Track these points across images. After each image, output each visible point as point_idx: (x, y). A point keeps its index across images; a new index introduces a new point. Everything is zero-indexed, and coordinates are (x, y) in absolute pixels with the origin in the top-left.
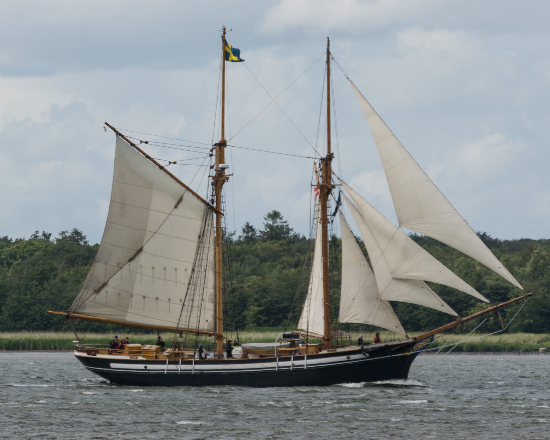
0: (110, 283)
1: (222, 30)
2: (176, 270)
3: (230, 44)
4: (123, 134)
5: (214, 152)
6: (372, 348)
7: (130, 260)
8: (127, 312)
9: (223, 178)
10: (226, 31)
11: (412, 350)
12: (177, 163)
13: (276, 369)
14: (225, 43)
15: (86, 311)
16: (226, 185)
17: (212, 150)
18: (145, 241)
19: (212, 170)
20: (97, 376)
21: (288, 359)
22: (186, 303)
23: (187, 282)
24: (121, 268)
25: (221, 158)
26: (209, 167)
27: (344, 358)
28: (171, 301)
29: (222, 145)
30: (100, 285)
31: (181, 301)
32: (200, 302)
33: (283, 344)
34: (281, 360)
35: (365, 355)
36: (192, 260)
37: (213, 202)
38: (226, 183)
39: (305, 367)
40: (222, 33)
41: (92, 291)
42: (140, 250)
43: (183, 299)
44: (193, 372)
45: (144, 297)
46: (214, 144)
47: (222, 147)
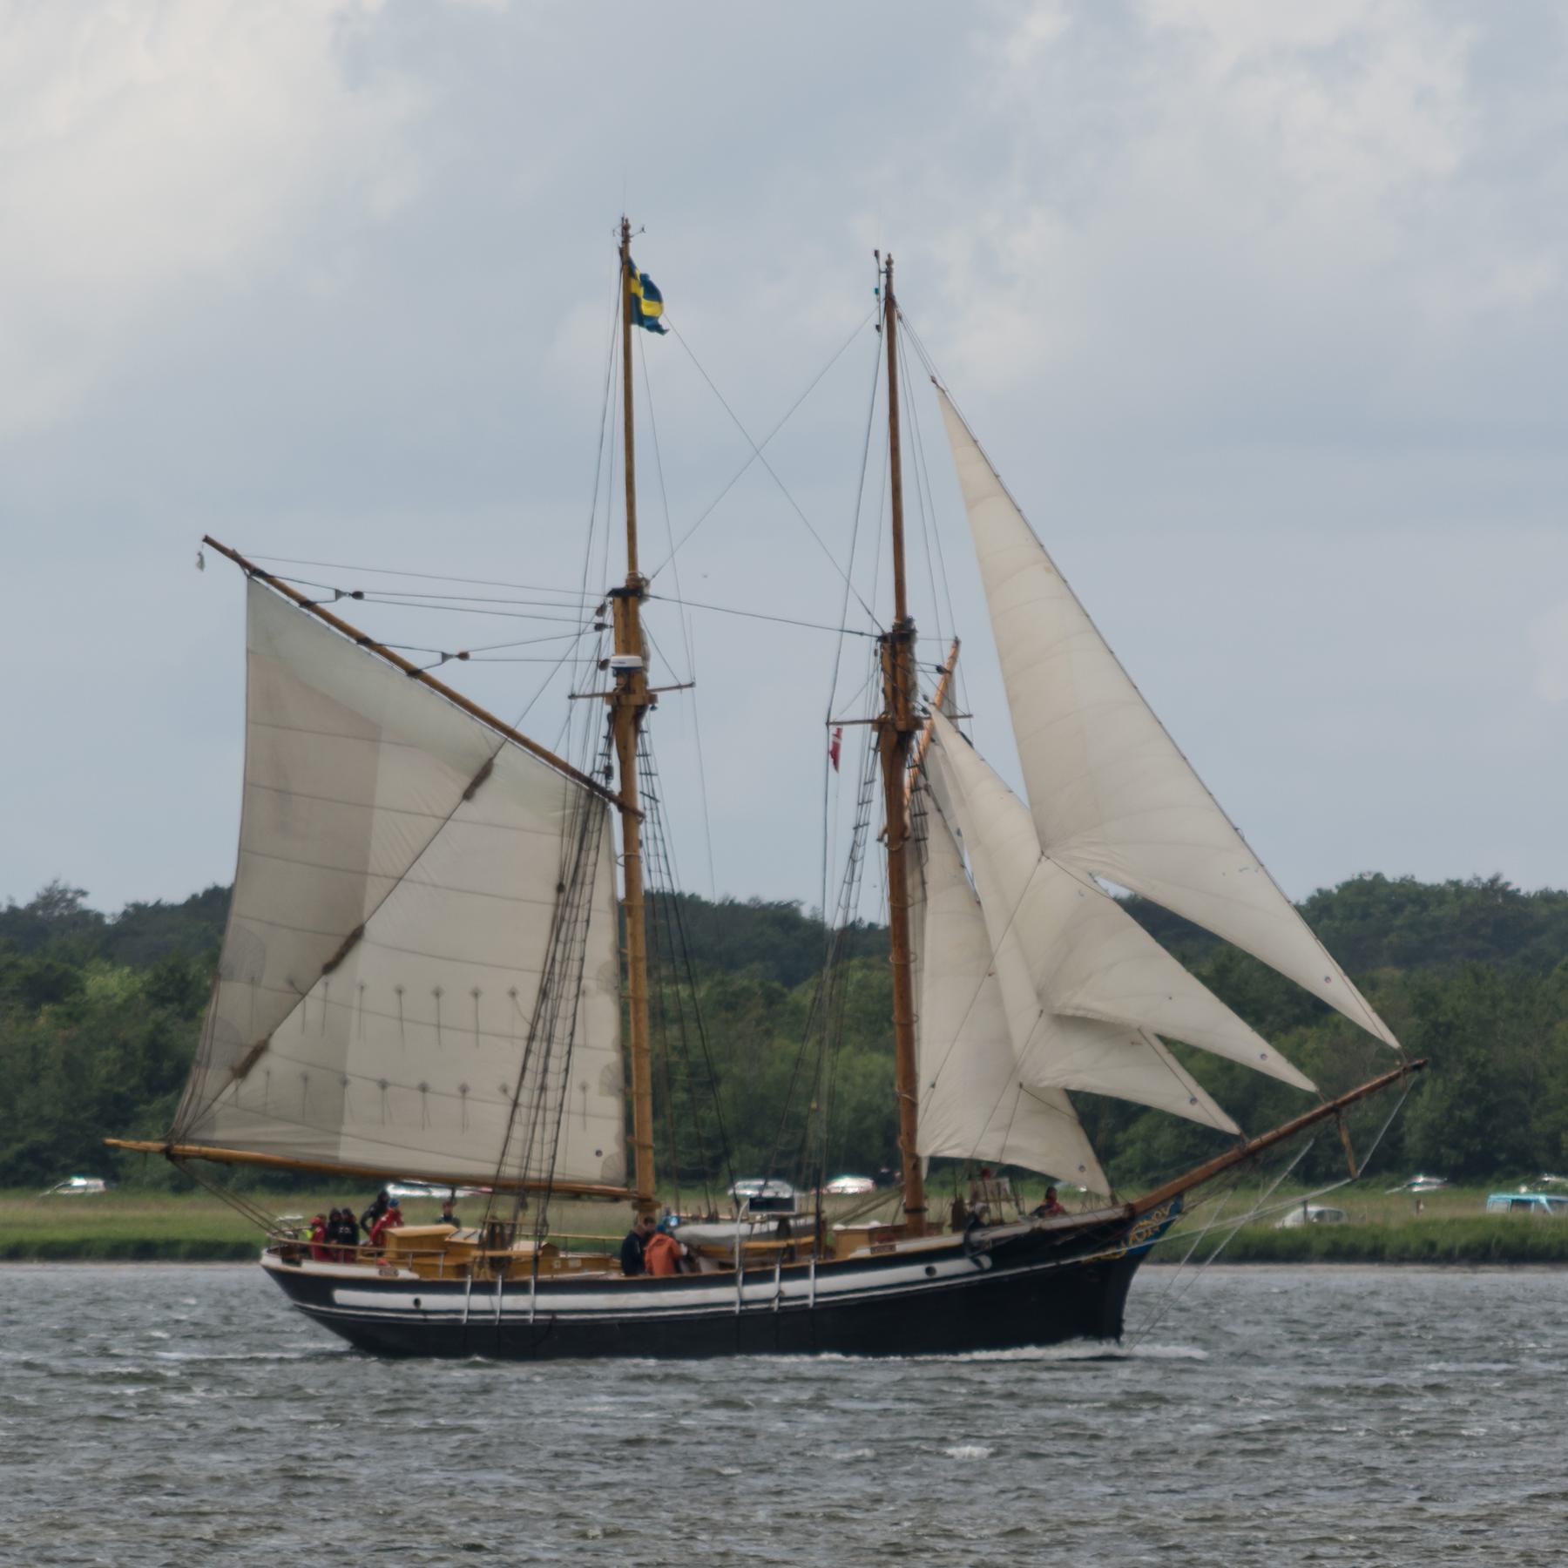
0: (276, 1043)
1: (619, 230)
2: (476, 994)
3: (640, 269)
4: (268, 571)
5: (609, 618)
6: (994, 1241)
7: (330, 967)
8: (338, 1133)
9: (636, 700)
10: (631, 232)
11: (1126, 1242)
12: (472, 655)
13: (737, 1308)
14: (628, 267)
15: (220, 1135)
16: (650, 720)
17: (601, 611)
18: (368, 906)
19: (601, 673)
20: (324, 1331)
21: (766, 1277)
22: (524, 1099)
23: (524, 1030)
24: (303, 995)
25: (631, 637)
26: (594, 665)
27: (916, 1272)
28: (470, 1094)
29: (631, 594)
30: (246, 1052)
31: (505, 1090)
32: (536, 1093)
33: (757, 1228)
34: (750, 1278)
35: (977, 1262)
36: (537, 962)
37: (608, 772)
38: (649, 714)
39: (810, 1302)
40: (619, 239)
41: (225, 1073)
42: (356, 936)
43: (513, 1086)
44: (531, 1317)
45: (383, 1085)
46: (608, 590)
47: (631, 600)
